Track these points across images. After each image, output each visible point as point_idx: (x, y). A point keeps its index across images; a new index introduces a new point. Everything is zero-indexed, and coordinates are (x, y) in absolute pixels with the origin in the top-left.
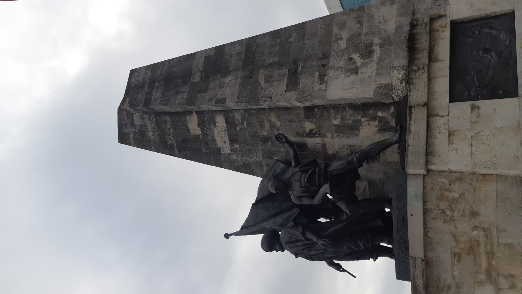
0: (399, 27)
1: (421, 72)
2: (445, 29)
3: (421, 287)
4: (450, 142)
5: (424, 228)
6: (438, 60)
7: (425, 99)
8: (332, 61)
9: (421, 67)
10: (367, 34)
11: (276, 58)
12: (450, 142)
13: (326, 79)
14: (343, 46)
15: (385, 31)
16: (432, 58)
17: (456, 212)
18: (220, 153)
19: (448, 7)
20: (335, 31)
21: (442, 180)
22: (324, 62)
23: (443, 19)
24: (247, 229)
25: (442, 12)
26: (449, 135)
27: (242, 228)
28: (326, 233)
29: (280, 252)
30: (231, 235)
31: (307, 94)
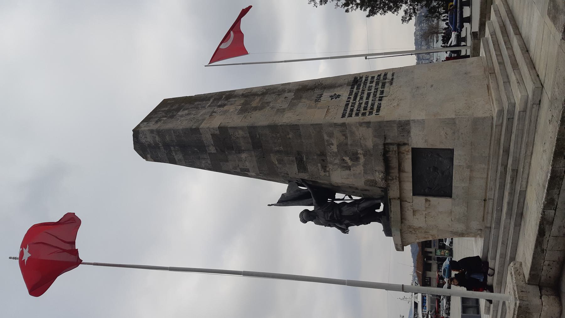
0: (375, 146)
1: (394, 181)
4: (414, 215)
6: (404, 171)
7: (398, 196)
9: (394, 178)
10: (351, 145)
12: (414, 215)
13: (328, 169)
15: (365, 146)
16: (401, 170)
19: (410, 138)
20: (326, 138)
22: (323, 158)
23: (407, 146)
25: (406, 142)
26: (414, 211)
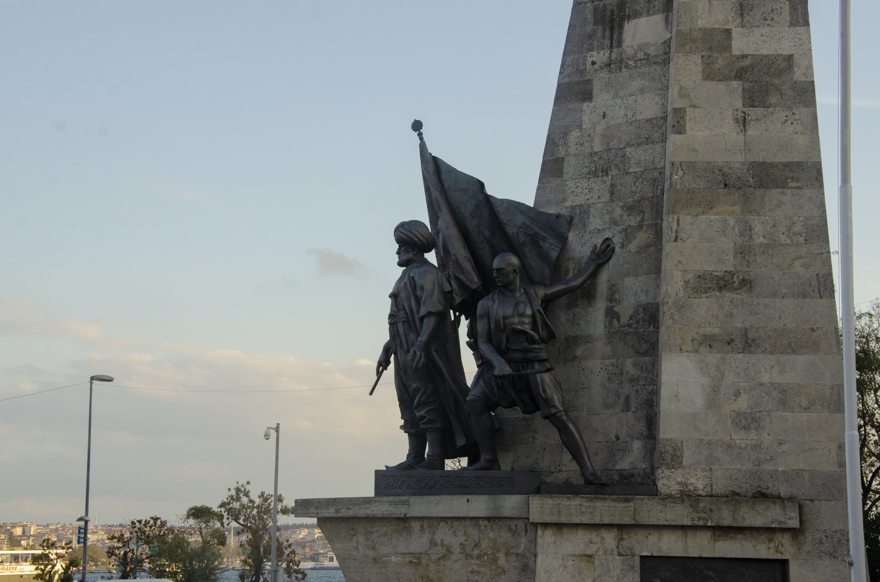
2: (772, 550)
3: (368, 512)
5: (452, 518)
8: (739, 359)
11: (761, 240)
14: (765, 378)
17: (478, 562)
18: (583, 100)
21: (523, 542)
24: (438, 175)
26: (589, 556)
27: (435, 159)
28: (434, 354)
29: (396, 259)
30: (420, 135)
31: (676, 317)
